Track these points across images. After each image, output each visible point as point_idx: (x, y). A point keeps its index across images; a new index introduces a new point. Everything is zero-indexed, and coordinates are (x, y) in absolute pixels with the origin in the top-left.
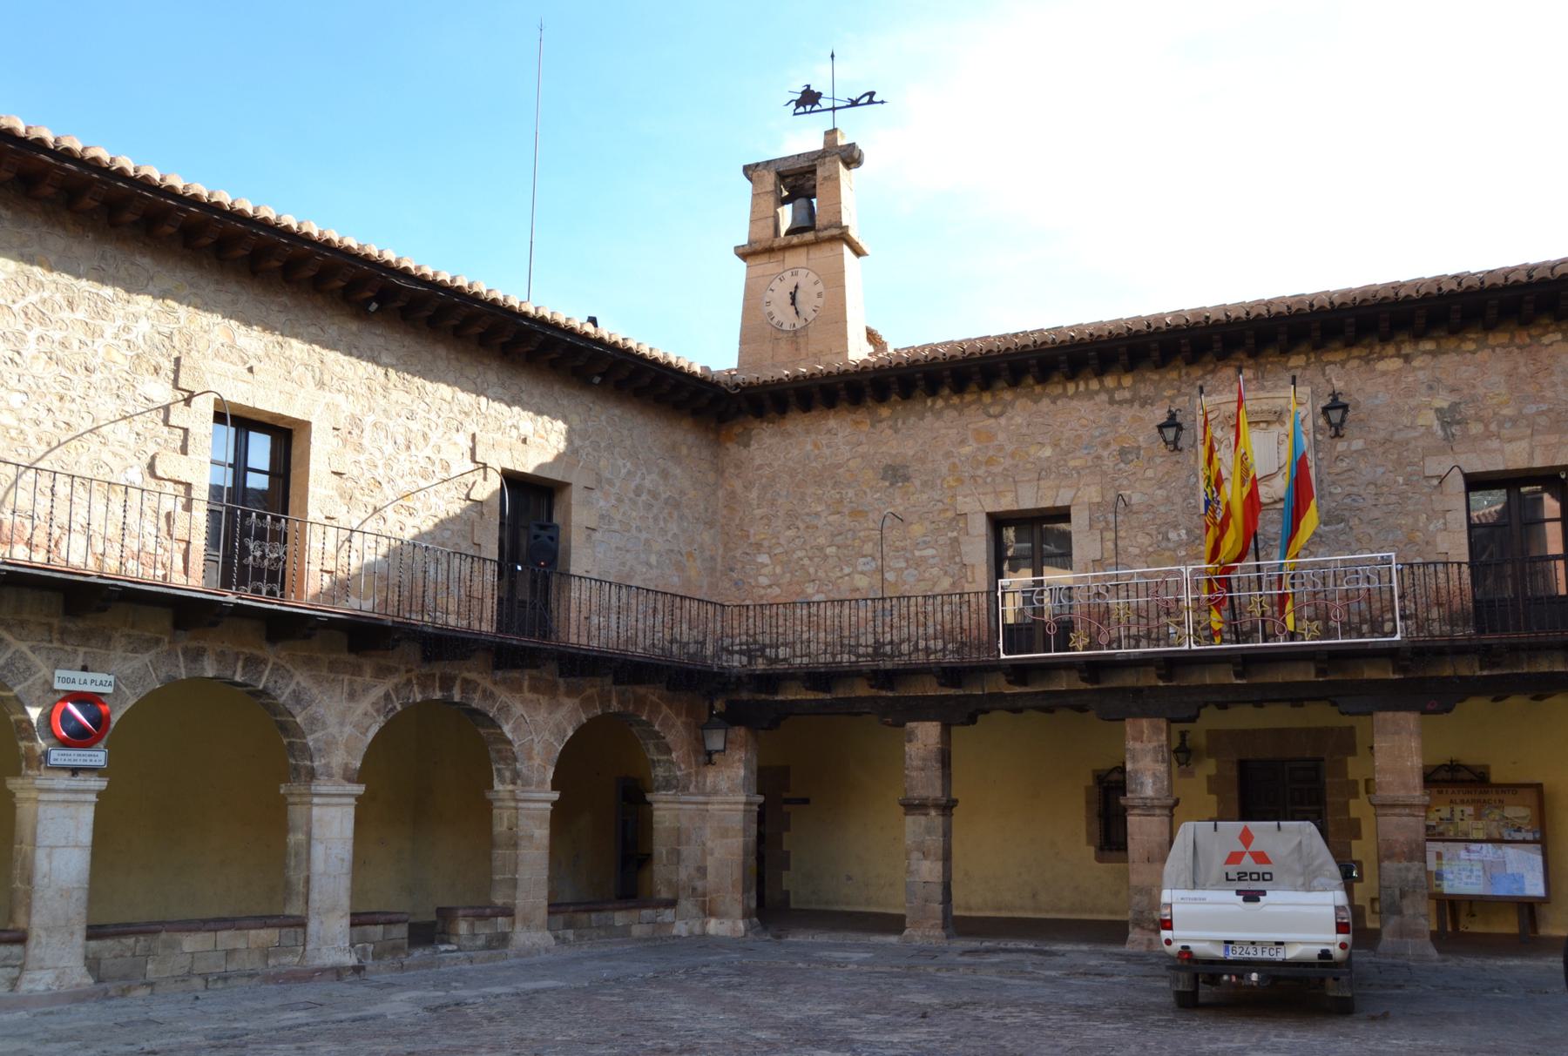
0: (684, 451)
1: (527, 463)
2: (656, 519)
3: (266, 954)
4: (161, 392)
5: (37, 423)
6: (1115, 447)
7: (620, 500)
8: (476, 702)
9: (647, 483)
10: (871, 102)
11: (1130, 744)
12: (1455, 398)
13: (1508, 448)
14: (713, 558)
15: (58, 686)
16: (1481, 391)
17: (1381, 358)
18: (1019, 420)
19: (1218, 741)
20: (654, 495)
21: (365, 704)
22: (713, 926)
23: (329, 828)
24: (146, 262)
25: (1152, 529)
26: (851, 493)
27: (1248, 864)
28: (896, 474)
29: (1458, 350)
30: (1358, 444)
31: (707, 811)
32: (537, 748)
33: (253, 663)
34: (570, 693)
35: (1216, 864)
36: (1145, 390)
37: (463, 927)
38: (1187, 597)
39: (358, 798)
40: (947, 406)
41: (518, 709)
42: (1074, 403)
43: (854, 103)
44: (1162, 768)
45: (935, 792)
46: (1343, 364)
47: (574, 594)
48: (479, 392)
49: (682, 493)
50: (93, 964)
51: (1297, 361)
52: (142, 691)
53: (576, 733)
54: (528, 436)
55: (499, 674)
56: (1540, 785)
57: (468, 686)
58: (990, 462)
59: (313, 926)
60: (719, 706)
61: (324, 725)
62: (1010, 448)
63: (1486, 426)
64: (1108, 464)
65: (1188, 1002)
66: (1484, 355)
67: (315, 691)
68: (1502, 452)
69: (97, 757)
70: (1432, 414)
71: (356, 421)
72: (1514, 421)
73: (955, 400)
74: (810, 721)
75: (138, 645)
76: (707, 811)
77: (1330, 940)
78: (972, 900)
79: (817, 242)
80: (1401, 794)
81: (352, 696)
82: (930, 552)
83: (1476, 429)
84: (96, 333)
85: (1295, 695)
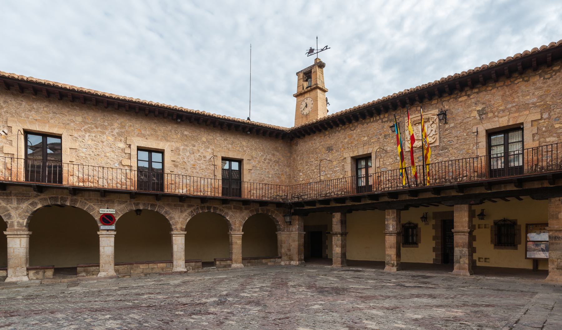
0: (280, 148)
2: (271, 166)
5: (90, 155)
6: (383, 135)
7: (259, 162)
8: (218, 212)
9: (268, 157)
10: (327, 49)
11: (386, 217)
12: (484, 106)
13: (501, 120)
14: (290, 175)
15: (101, 212)
16: (493, 102)
17: (460, 97)
18: (359, 130)
19: (436, 215)
20: (270, 160)
23: (179, 242)
24: (116, 116)
25: (393, 157)
26: (320, 155)
28: (330, 149)
29: (486, 90)
30: (452, 125)
31: (291, 237)
32: (237, 222)
33: (152, 205)
34: (246, 209)
37: (217, 263)
39: (185, 235)
40: (342, 129)
41: (231, 213)
42: (373, 124)
43: (322, 50)
44: (395, 223)
46: (448, 101)
47: (246, 186)
49: (279, 159)
50: (116, 271)
51: (434, 102)
52: (124, 213)
53: (249, 218)
55: (224, 206)
57: (215, 208)
58: (352, 143)
59: (175, 263)
60: (292, 211)
61: (174, 219)
62: (356, 138)
63: (494, 114)
64: (381, 140)
66: (494, 91)
67: (171, 211)
68: (499, 121)
69: (113, 227)
70: (476, 112)
72: (503, 111)
73: (343, 127)
75: (121, 203)
78: (349, 257)
80: (461, 229)
82: (338, 169)
83: (490, 115)
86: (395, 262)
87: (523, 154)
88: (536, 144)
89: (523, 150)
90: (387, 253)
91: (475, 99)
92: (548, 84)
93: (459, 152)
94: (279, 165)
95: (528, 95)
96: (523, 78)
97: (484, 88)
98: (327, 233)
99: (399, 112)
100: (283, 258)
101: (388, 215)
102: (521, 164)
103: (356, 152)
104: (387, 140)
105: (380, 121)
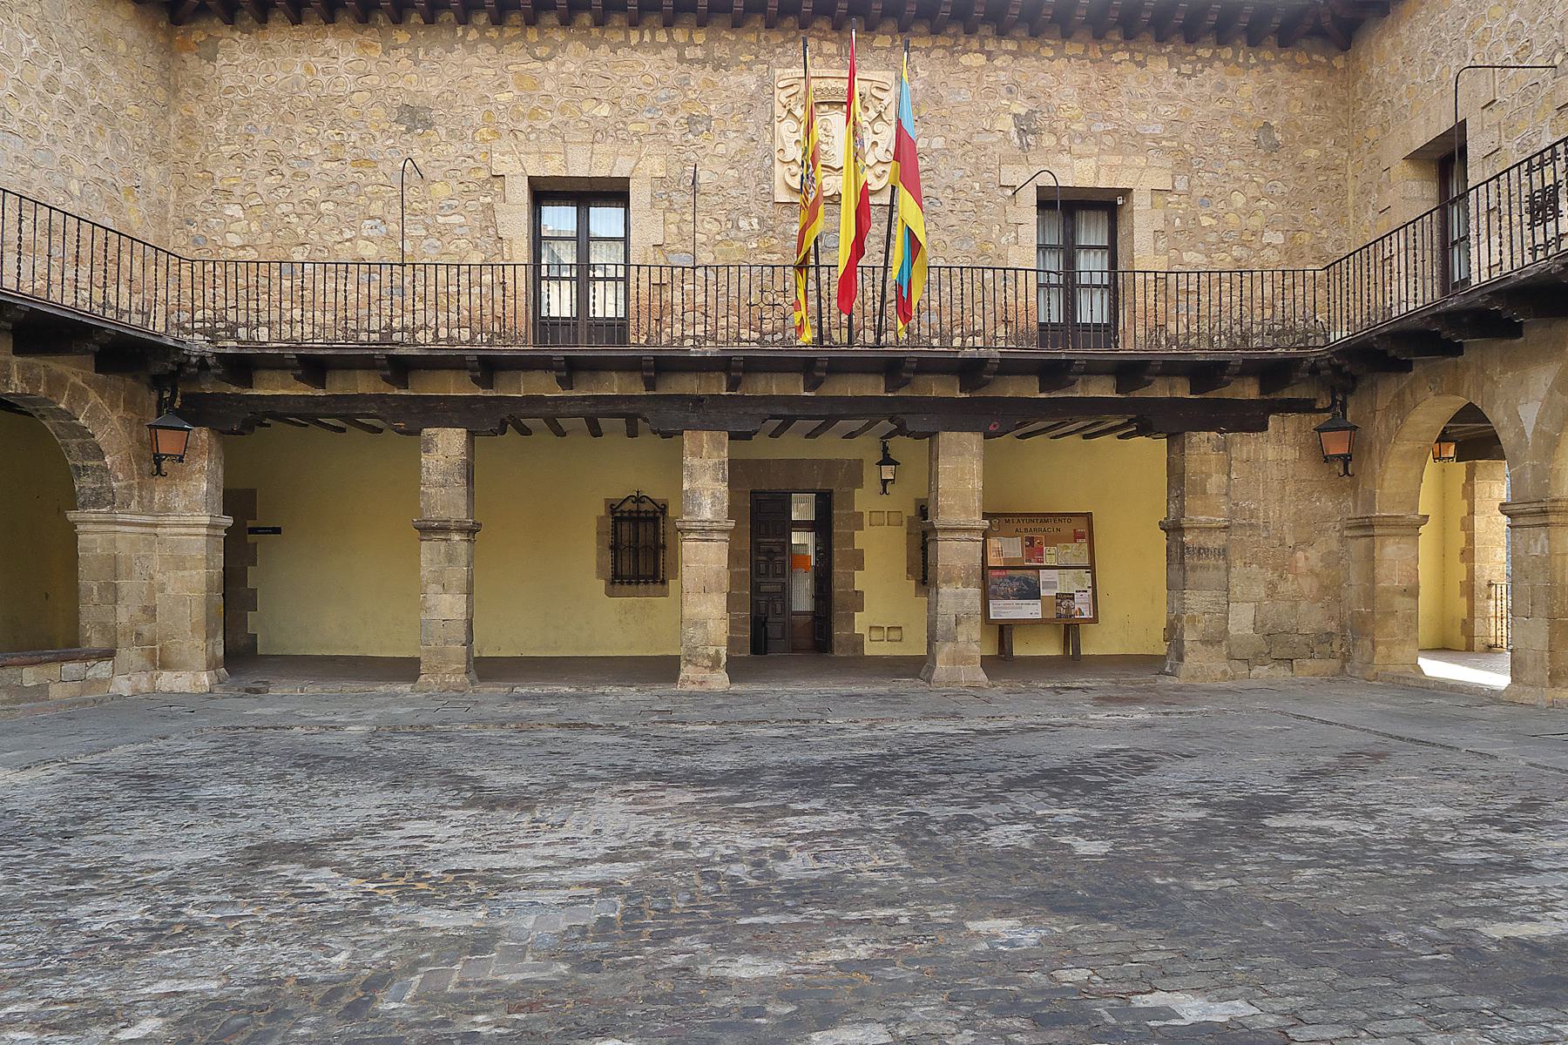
0: (122, 48)
7: (21, 89)
11: (688, 460)
12: (1031, 105)
22: (168, 681)
28: (414, 117)
36: (720, 51)
40: (483, 39)
42: (638, 55)
44: (723, 487)
58: (534, 114)
62: (559, 101)
64: (675, 134)
80: (959, 519)
82: (456, 219)
83: (1049, 141)
86: (723, 651)
87: (626, 279)
88: (1161, 264)
89: (627, 265)
90: (687, 611)
91: (1009, 74)
92: (1187, 91)
93: (957, 244)
94: (117, 138)
95: (1144, 109)
96: (1132, 53)
97: (1032, 47)
98: (253, 531)
99: (752, 38)
100: (123, 652)
101: (697, 454)
102: (621, 314)
103: (558, 159)
104: (700, 140)
105: (672, 53)
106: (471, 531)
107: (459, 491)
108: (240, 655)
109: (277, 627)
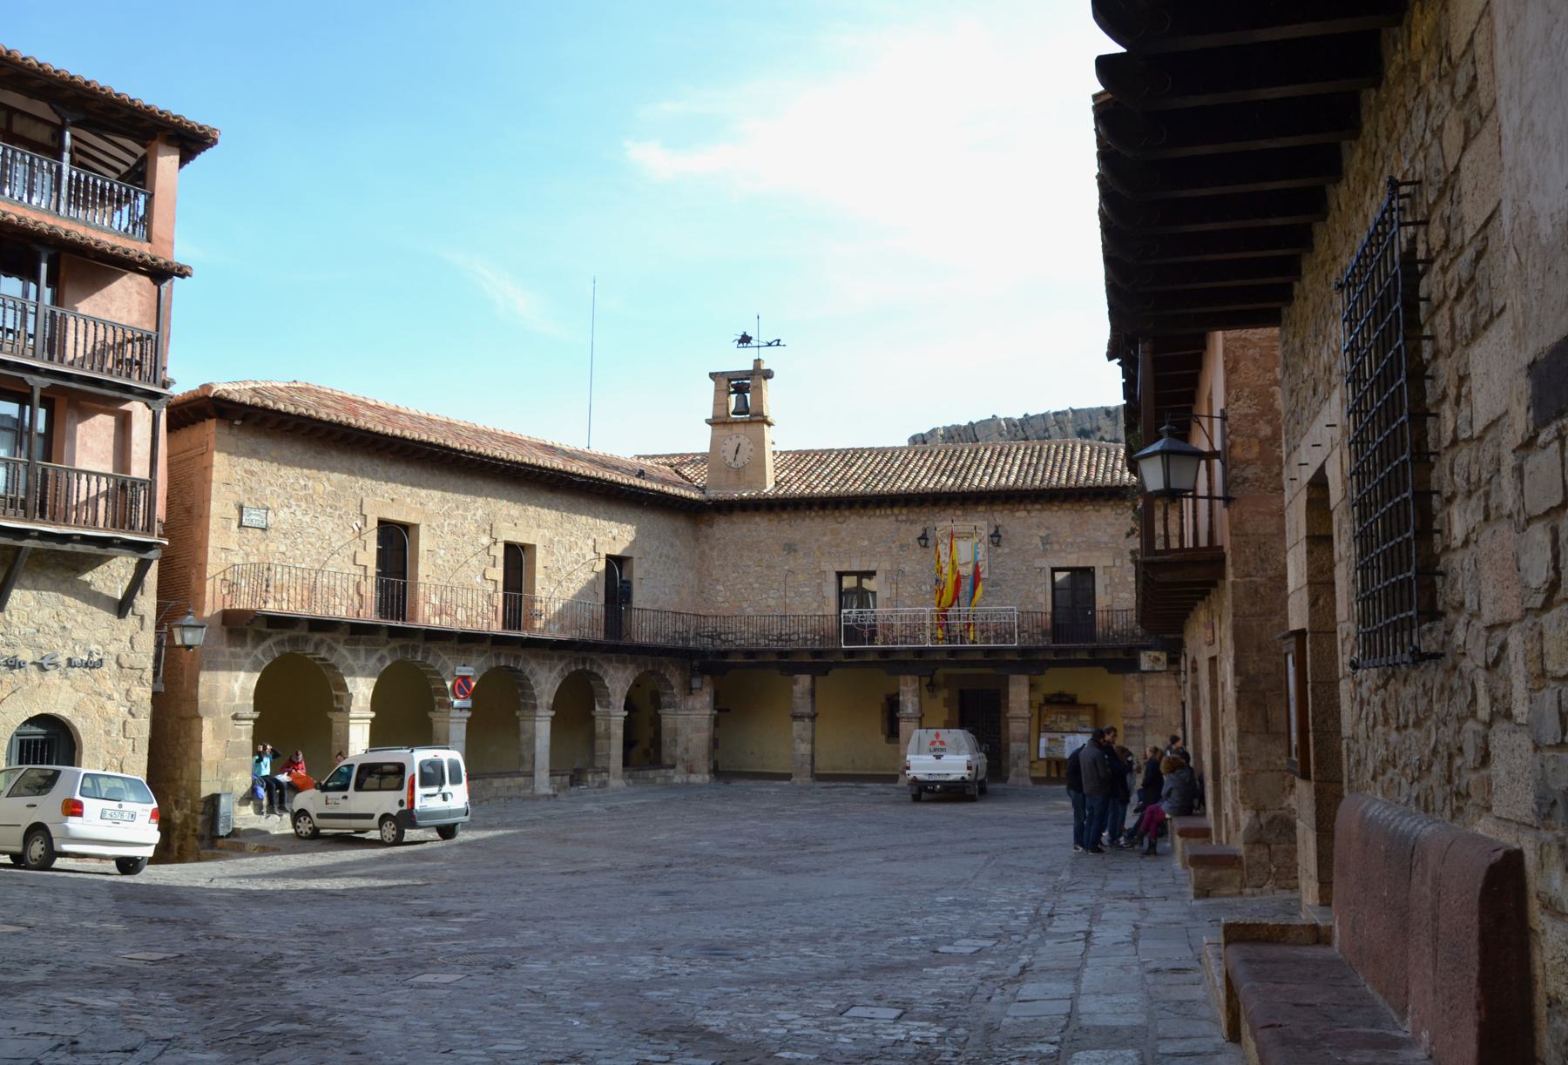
1: (617, 550)
3: (520, 788)
4: (485, 540)
8: (595, 670)
21: (554, 674)
22: (694, 778)
23: (542, 729)
24: (480, 482)
27: (938, 745)
28: (790, 548)
30: (1007, 550)
33: (517, 658)
35: (927, 746)
36: (912, 517)
37: (590, 778)
38: (928, 622)
41: (611, 671)
45: (808, 710)
48: (596, 517)
51: (981, 508)
54: (618, 534)
56: (1095, 706)
58: (838, 546)
60: (696, 663)
65: (917, 799)
71: (551, 541)
74: (738, 673)
76: (690, 719)
77: (964, 772)
78: (823, 766)
79: (750, 422)
81: (550, 670)
83: (1056, 547)
84: (465, 518)
85: (973, 664)
106: (813, 718)
107: (808, 700)
108: (718, 773)
109: (245, 523)
